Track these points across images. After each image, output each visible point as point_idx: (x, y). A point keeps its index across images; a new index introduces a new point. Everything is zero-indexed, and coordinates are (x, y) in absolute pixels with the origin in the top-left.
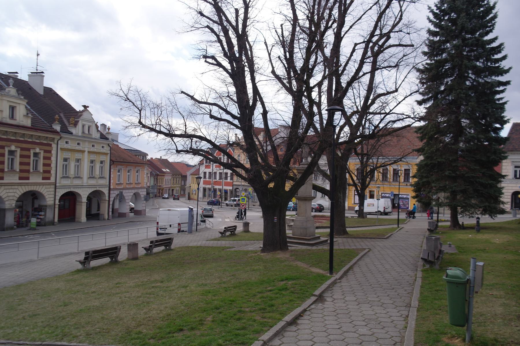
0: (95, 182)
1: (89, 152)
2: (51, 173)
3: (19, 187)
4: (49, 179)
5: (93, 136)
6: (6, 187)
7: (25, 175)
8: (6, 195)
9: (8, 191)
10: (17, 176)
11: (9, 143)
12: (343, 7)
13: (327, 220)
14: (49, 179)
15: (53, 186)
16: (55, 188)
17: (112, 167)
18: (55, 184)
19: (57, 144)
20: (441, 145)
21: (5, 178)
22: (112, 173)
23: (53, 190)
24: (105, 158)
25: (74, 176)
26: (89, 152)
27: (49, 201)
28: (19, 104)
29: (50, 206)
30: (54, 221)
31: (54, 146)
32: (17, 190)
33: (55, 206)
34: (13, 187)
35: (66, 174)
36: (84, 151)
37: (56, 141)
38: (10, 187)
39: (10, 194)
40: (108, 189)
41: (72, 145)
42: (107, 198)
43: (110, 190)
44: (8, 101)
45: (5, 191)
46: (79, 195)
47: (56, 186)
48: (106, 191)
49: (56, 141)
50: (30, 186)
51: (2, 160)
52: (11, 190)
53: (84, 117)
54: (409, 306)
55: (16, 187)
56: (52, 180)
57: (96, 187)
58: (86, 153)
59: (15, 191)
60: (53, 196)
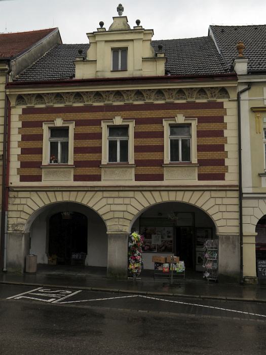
3: (138, 195)
4: (221, 177)
6: (106, 194)
7: (33, 172)
8: (216, 209)
9: (110, 201)
10: (132, 173)
11: (109, 114)
14: (221, 177)
15: (236, 194)
18: (239, 188)
20: (192, 232)
21: (103, 178)
23: (236, 201)
27: (225, 225)
28: (132, 40)
29: (227, 237)
30: (241, 273)
31: (229, 106)
32: (29, 199)
33: (241, 240)
34: (122, 194)
37: (233, 96)
38: (115, 194)
39: (114, 208)
44: (106, 41)
45: (104, 201)
46: (99, 222)
47: (241, 194)
49: (233, 96)
50: (163, 194)
51: (98, 145)
54: (51, 47)
55: (131, 194)
56: (231, 178)
59: (127, 201)
60: (237, 215)
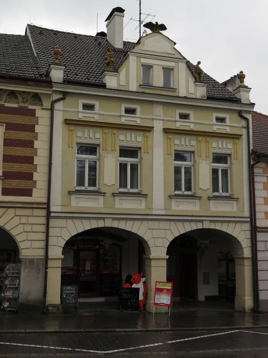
0: (143, 207)
1: (166, 131)
2: (34, 179)
4: (29, 193)
5: (182, 92)
12: (141, 347)
13: (256, 173)
15: (43, 213)
16: (48, 216)
17: (256, 170)
18: (47, 206)
19: (52, 110)
22: (258, 186)
24: (230, 146)
25: (211, 193)
26: (166, 131)
29: (32, 261)
31: (42, 115)
33: (46, 264)
35: (226, 189)
36: (149, 129)
37: (47, 104)
40: (247, 227)
41: (114, 113)
42: (247, 253)
43: (254, 230)
47: (49, 212)
48: (241, 234)
49: (47, 104)
52: (35, 210)
53: (144, 48)
56: (38, 195)
57: (202, 221)
58: (158, 136)
60: (42, 236)
